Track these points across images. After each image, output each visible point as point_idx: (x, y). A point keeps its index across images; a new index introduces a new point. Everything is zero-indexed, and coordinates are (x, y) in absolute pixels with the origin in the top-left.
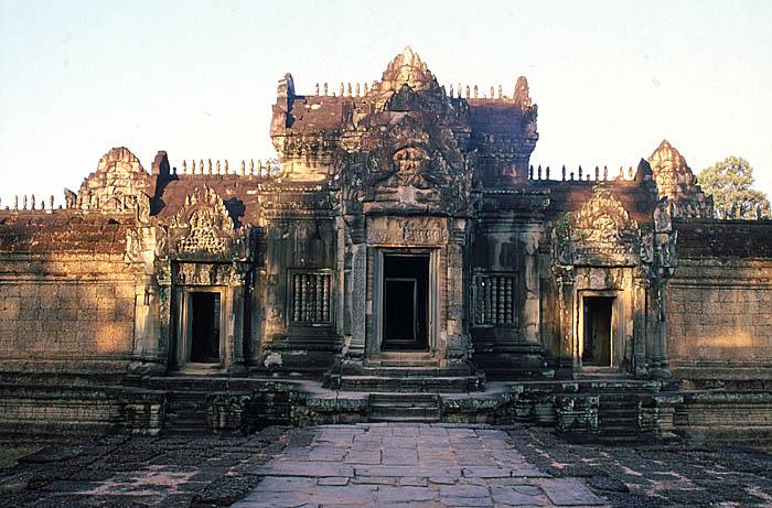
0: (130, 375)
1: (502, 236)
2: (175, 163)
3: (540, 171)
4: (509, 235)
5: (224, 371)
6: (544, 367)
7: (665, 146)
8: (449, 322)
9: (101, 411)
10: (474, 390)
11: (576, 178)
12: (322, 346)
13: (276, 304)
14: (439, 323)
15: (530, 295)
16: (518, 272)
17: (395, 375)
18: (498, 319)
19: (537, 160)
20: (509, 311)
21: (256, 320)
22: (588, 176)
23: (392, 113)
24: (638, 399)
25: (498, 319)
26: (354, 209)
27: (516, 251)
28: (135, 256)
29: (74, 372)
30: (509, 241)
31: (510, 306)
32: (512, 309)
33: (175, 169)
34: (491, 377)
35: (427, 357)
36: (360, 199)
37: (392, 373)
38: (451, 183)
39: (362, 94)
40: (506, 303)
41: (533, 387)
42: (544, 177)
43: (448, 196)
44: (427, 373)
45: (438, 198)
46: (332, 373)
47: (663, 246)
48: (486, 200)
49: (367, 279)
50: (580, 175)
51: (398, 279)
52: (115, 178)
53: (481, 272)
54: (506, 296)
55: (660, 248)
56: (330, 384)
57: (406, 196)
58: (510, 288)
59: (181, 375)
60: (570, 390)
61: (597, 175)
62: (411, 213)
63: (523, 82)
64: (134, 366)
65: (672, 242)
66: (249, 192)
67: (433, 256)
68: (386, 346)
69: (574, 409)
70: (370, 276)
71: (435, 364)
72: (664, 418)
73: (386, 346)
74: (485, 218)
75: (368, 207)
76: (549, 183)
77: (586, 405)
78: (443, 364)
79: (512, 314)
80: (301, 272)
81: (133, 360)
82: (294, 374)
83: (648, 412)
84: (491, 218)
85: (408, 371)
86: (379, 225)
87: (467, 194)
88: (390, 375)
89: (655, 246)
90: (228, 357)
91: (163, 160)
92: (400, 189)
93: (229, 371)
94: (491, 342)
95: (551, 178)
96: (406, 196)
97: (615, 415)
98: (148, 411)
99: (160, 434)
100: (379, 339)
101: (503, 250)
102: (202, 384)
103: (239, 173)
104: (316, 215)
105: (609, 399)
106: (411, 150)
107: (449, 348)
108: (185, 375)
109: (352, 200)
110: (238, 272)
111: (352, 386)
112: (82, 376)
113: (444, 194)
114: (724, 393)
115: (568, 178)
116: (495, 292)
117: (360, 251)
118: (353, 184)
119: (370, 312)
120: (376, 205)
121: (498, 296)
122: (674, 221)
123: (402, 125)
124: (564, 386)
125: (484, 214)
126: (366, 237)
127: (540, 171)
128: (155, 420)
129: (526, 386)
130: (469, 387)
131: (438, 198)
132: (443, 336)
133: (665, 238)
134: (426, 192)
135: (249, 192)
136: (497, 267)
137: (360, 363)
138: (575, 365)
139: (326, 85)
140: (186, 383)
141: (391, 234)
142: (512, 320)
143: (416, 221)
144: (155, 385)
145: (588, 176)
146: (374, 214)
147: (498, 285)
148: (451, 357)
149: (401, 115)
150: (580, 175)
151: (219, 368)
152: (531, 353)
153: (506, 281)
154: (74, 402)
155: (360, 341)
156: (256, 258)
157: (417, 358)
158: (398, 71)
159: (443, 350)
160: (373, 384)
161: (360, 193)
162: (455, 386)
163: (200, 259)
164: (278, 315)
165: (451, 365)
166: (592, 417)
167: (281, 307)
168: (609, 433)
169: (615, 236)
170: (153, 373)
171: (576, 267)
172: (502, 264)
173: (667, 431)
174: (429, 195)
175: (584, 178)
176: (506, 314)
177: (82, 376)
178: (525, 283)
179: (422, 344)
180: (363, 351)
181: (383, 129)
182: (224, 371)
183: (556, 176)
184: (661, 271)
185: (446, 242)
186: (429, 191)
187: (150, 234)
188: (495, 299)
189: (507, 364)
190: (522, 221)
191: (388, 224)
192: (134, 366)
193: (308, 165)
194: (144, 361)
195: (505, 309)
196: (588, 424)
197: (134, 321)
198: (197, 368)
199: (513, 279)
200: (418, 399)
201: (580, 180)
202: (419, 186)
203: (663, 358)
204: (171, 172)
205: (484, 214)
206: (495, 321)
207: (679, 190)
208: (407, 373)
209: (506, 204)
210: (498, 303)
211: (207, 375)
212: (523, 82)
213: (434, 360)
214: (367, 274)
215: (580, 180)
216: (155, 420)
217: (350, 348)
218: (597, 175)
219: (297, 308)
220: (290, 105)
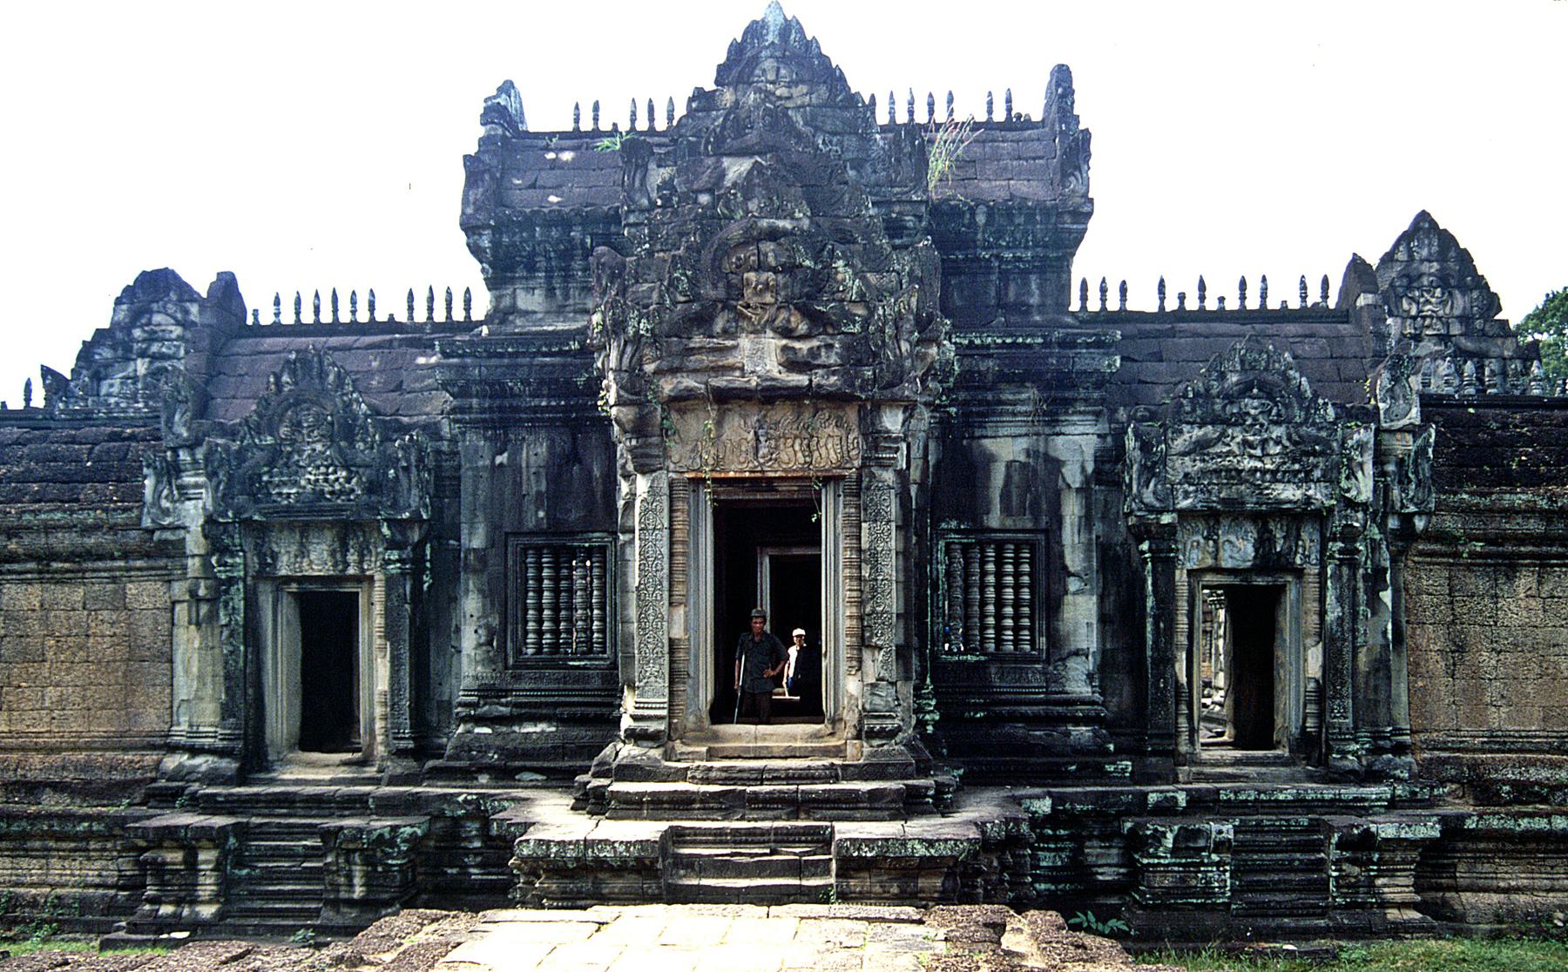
0: (162, 783)
1: (1006, 447)
2: (258, 304)
3: (1103, 290)
4: (1023, 443)
5: (371, 771)
6: (1107, 753)
7: (1424, 225)
8: (867, 655)
9: (98, 865)
10: (924, 812)
11: (1192, 304)
12: (591, 711)
13: (484, 615)
14: (844, 653)
15: (1073, 585)
16: (1046, 531)
17: (734, 781)
18: (999, 641)
19: (1086, 265)
20: (1026, 622)
21: (441, 651)
22: (1222, 300)
23: (726, 162)
24: (1331, 829)
25: (999, 641)
26: (635, 387)
27: (1040, 477)
28: (166, 512)
29: (42, 777)
30: (1022, 458)
31: (1026, 610)
32: (1031, 617)
33: (256, 313)
34: (976, 781)
35: (816, 736)
36: (649, 368)
37: (729, 777)
38: (866, 322)
39: (661, 124)
40: (1017, 604)
41: (1074, 798)
42: (1113, 305)
43: (860, 352)
44: (807, 776)
45: (833, 359)
46: (595, 775)
47: (1401, 463)
48: (966, 361)
49: (671, 555)
50: (1202, 298)
51: (796, 552)
52: (152, 338)
53: (957, 531)
54: (1017, 587)
55: (1391, 468)
56: (594, 803)
57: (760, 357)
58: (1026, 568)
59: (272, 782)
60: (1167, 809)
61: (1243, 298)
62: (770, 395)
63: (1062, 78)
64: (172, 762)
65: (1421, 452)
66: (421, 360)
67: (827, 498)
68: (722, 711)
69: (1174, 852)
70: (678, 548)
71: (838, 752)
72: (1391, 874)
73: (722, 711)
74: (966, 403)
75: (667, 386)
76: (1124, 317)
77: (1201, 843)
78: (858, 752)
79: (1031, 629)
80: (540, 541)
81: (173, 749)
82: (527, 776)
83: (1353, 862)
84: (980, 403)
85: (762, 771)
86: (699, 424)
87: (905, 346)
88: (724, 781)
89: (1379, 461)
90: (379, 739)
91: (227, 287)
92: (745, 342)
93: (380, 771)
94: (980, 695)
95: (1132, 306)
96: (758, 353)
97: (289, 854)
98: (191, 864)
99: (221, 915)
100: (706, 694)
101: (1008, 477)
102: (318, 803)
103: (402, 317)
104: (567, 409)
105: (1259, 829)
106: (767, 247)
107: (866, 714)
108: (284, 783)
109: (630, 370)
110: (392, 544)
111: (633, 807)
112: (59, 787)
113: (847, 347)
114: (1548, 815)
115: (1171, 305)
116: (991, 579)
117: (652, 491)
118: (631, 331)
119: (678, 632)
120: (689, 382)
121: (999, 587)
122: (1430, 403)
123: (746, 186)
124: (1153, 798)
125: (962, 395)
126: (667, 456)
127: (1103, 290)
128: (207, 885)
129: (1058, 800)
130: (909, 805)
131: (833, 359)
132: (852, 685)
133: (1404, 445)
134: (803, 346)
135: (421, 360)
136: (994, 519)
137: (656, 753)
138: (1183, 748)
139: (596, 108)
140: (287, 801)
141: (738, 449)
142: (1032, 642)
143: (783, 415)
144: (210, 805)
145: (1222, 300)
146: (682, 401)
147: (999, 563)
148: (872, 735)
149: (745, 165)
150: (1202, 298)
151: (363, 763)
152: (1077, 722)
153: (1017, 551)
154: (37, 844)
155: (658, 700)
156: (438, 512)
157: (795, 738)
158: (755, 60)
159: (851, 718)
160: (681, 804)
161: (648, 352)
162: (872, 807)
163: (307, 518)
164: (490, 643)
165: (873, 755)
166: (1221, 878)
167: (495, 621)
168: (1263, 910)
169: (1278, 442)
170: (212, 778)
171: (1184, 514)
172: (1007, 510)
173: (1402, 906)
174: (814, 353)
175: (1211, 305)
176: (1017, 629)
177: (59, 787)
178: (1062, 556)
179: (807, 703)
180: (662, 726)
181: (704, 199)
182: (371, 771)
183: (1143, 301)
184: (1393, 523)
185: (857, 463)
186: (815, 343)
187: (195, 461)
188: (991, 593)
189: (1029, 748)
190: (1052, 415)
191: (719, 423)
192: (172, 762)
193: (550, 292)
194: (194, 751)
195: (1017, 617)
196: (1207, 891)
197: (171, 661)
198: (311, 765)
199: (1033, 547)
200: (740, 838)
201: (1202, 309)
202: (786, 332)
203: (1398, 731)
204: (250, 321)
205: (962, 395)
206: (991, 646)
207: (1456, 329)
208: (760, 776)
209: (1021, 369)
210: (1000, 604)
211: (332, 782)
212: (1062, 78)
213: (833, 742)
214: (672, 543)
215: (1202, 309)
216: (207, 885)
217: (635, 718)
218: (1243, 298)
219: (531, 626)
220: (501, 115)
